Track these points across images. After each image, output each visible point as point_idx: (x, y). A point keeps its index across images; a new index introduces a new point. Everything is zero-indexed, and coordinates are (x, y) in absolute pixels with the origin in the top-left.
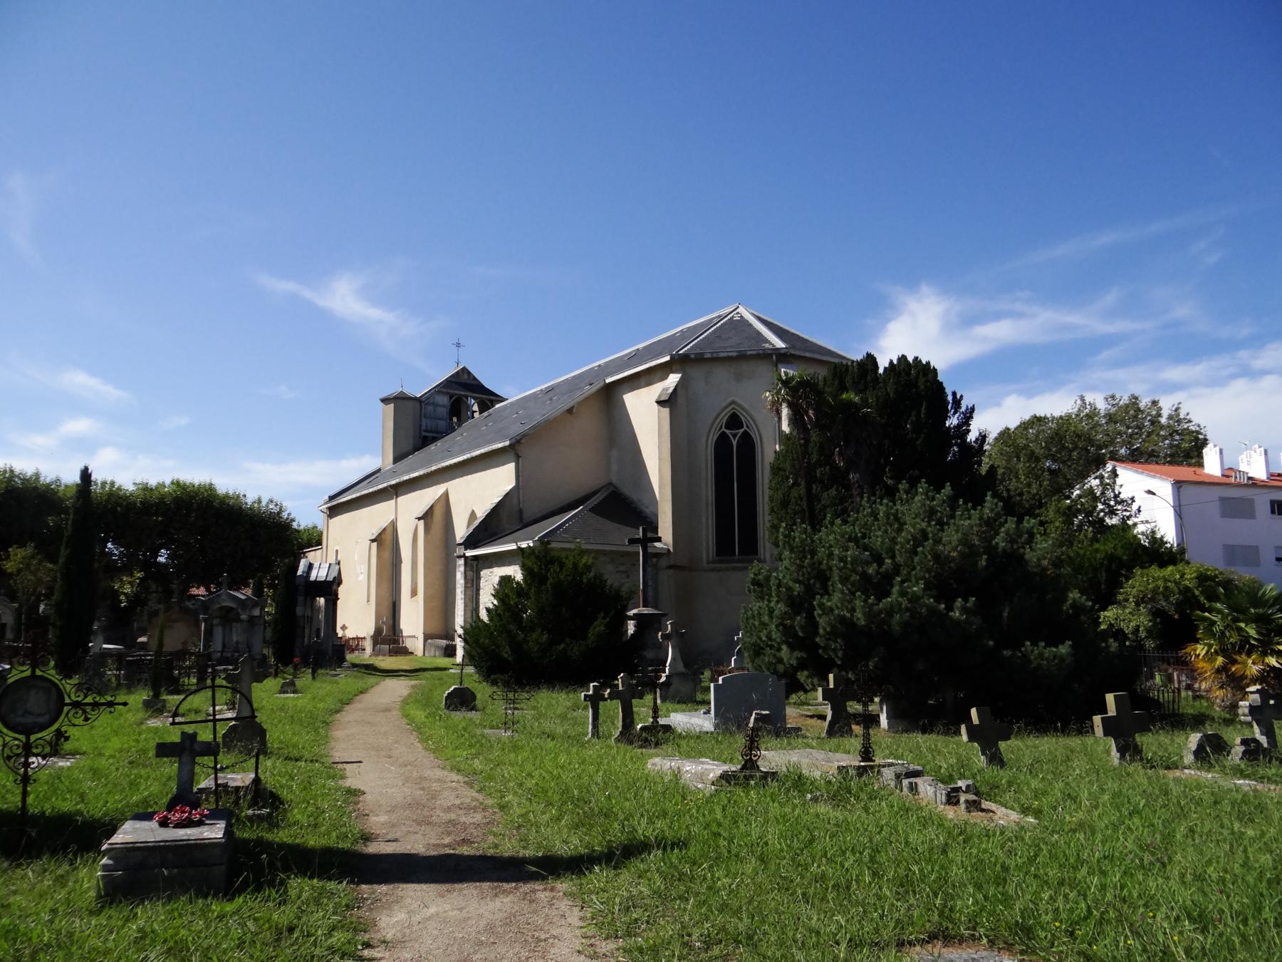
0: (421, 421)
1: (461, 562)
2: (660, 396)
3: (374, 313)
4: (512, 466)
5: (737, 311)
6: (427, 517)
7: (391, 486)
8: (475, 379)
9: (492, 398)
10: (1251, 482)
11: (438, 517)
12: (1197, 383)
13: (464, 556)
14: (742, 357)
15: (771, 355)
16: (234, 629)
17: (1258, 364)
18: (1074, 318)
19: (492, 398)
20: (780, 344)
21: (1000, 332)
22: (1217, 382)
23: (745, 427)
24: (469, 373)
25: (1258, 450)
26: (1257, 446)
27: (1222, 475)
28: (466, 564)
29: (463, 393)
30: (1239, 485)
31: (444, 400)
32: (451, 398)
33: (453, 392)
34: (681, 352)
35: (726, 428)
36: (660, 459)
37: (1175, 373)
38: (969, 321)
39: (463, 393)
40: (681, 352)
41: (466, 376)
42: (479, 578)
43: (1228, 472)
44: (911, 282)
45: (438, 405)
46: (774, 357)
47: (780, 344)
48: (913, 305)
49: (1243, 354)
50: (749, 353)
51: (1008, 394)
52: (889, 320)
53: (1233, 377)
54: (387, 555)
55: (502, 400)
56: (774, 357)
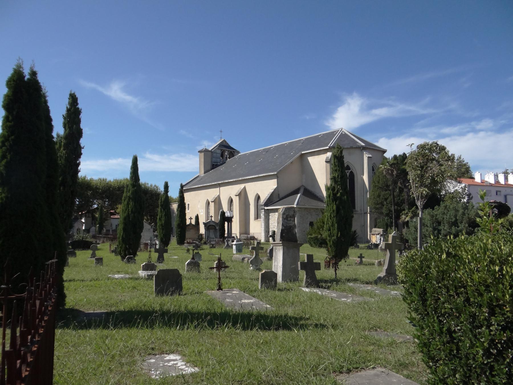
0: (212, 158)
1: (263, 210)
2: (326, 159)
3: (128, 98)
4: (276, 180)
5: (342, 130)
6: (239, 195)
7: (218, 184)
8: (228, 144)
9: (234, 151)
10: (490, 185)
11: (243, 195)
12: (454, 134)
13: (264, 209)
14: (352, 148)
15: (360, 148)
16: (210, 232)
17: (478, 127)
18: (412, 108)
19: (234, 151)
20: (363, 144)
21: (382, 112)
22: (462, 134)
23: (351, 170)
24: (226, 142)
25: (492, 174)
26: (491, 173)
27: (481, 182)
28: (265, 211)
29: (225, 149)
30: (487, 186)
31: (219, 152)
32: (221, 151)
33: (222, 149)
34: (331, 146)
35: (351, 171)
36: (327, 180)
37: (446, 130)
38: (370, 107)
39: (225, 149)
40: (331, 146)
41: (225, 143)
42: (269, 216)
43: (483, 181)
44: (350, 92)
45: (217, 153)
46: (362, 148)
47: (363, 144)
48: (349, 100)
49: (473, 123)
50: (354, 147)
51: (382, 137)
52: (339, 106)
53: (468, 132)
54: (217, 206)
55: (238, 152)
56: (362, 148)
